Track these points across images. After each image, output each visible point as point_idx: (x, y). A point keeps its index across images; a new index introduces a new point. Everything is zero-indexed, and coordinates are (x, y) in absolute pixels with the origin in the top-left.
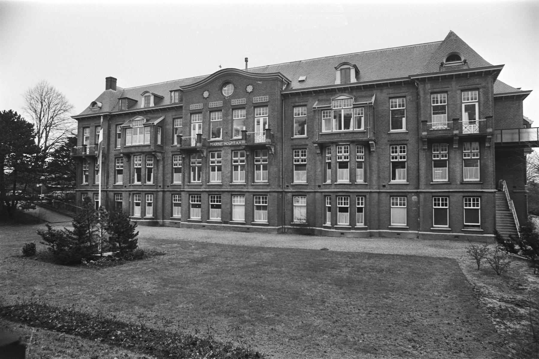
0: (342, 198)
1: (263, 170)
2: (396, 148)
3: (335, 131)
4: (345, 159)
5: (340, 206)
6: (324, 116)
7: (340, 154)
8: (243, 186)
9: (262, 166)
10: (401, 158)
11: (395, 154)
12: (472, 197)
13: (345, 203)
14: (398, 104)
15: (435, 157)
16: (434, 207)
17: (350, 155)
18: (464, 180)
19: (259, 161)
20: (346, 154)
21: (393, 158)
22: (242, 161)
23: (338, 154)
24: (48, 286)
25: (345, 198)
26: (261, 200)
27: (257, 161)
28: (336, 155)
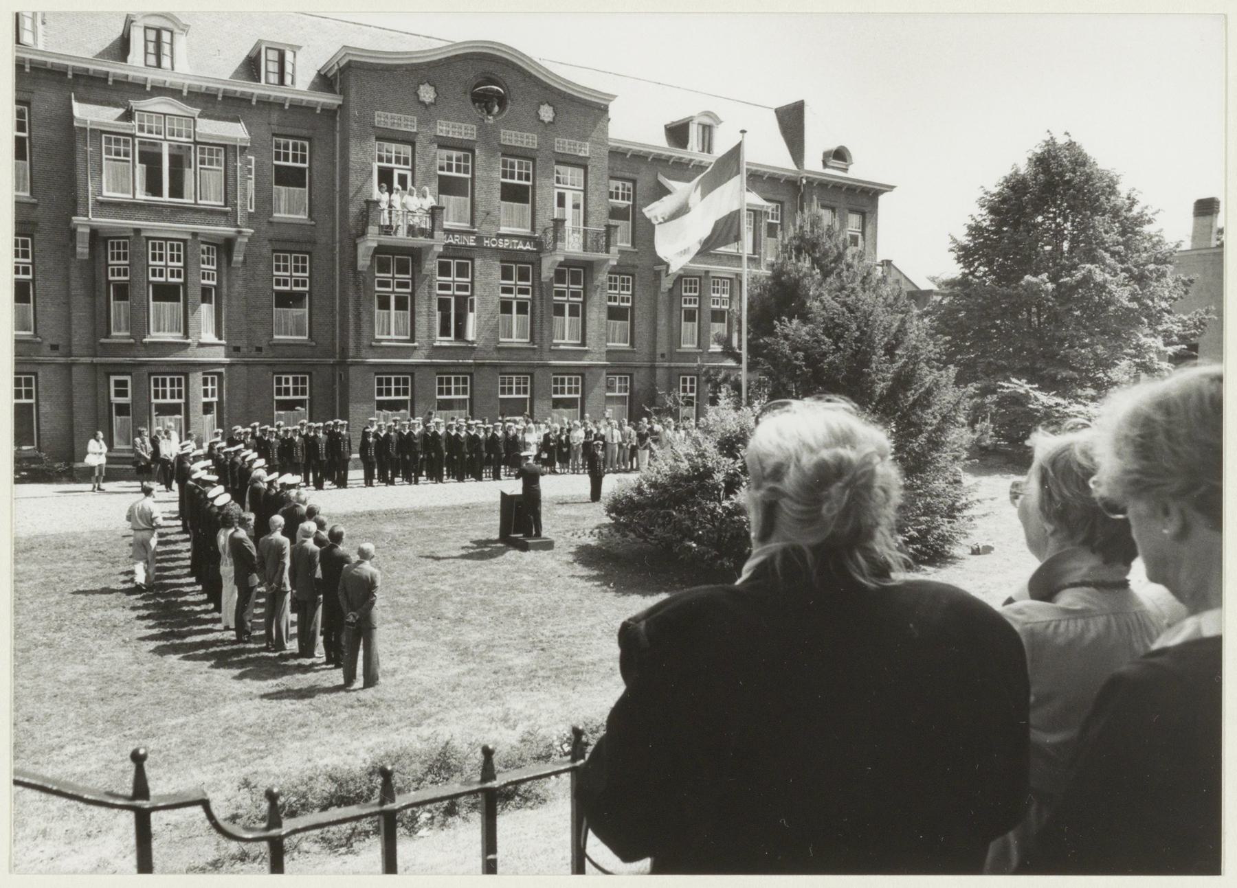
0: (164, 381)
1: (570, 315)
2: (285, 259)
3: (141, 196)
4: (172, 276)
5: (160, 401)
6: (109, 152)
7: (157, 263)
8: (531, 353)
9: (453, 300)
10: (297, 284)
11: (281, 273)
12: (168, 374)
13: (172, 392)
14: (394, 155)
15: (154, 275)
16: (276, 398)
17: (33, 264)
18: (276, 337)
19: (387, 284)
20: (175, 264)
21: (278, 283)
22: (522, 291)
23: (275, 273)
24: (39, 675)
25: (172, 381)
26: (168, 388)
27: (382, 284)
28: (108, 265)
